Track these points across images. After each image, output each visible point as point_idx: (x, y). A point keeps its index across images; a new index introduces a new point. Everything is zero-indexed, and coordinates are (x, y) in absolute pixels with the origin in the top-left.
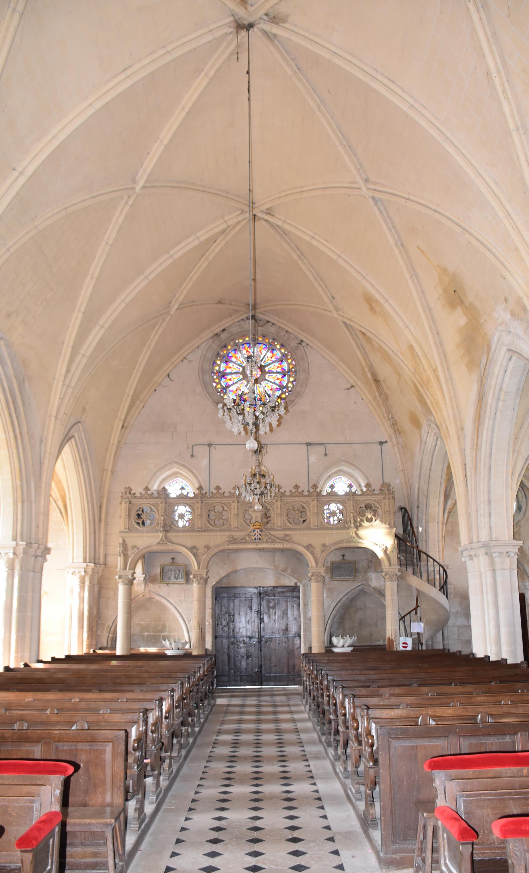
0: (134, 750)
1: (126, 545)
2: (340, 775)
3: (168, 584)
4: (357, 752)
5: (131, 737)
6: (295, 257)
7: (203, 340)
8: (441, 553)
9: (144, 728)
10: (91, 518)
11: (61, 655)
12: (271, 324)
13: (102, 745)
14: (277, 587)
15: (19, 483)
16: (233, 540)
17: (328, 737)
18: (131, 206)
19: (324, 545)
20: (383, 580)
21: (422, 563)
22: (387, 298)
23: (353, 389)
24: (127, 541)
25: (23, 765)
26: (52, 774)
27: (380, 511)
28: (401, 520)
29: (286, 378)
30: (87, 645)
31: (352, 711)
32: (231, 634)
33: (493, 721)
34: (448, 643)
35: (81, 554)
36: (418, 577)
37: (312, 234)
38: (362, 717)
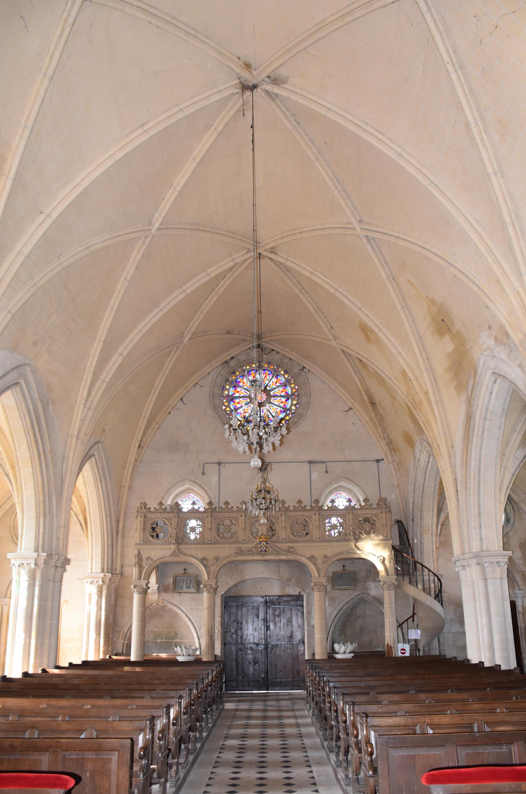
0: (141, 758)
1: (141, 557)
2: (342, 782)
3: (180, 593)
4: (357, 760)
5: (137, 745)
6: (297, 292)
7: (213, 367)
8: (435, 563)
9: (150, 736)
10: (109, 531)
11: (78, 661)
12: (276, 352)
13: (108, 754)
14: (282, 596)
15: (41, 498)
16: (240, 552)
17: (331, 742)
18: (148, 246)
19: (325, 556)
20: (381, 589)
21: (418, 573)
22: (381, 328)
23: (352, 411)
24: (142, 553)
25: (24, 778)
26: (53, 788)
27: (378, 525)
28: (398, 532)
29: (290, 401)
30: (103, 651)
31: (352, 718)
32: (239, 641)
33: (489, 730)
34: (444, 649)
35: (99, 565)
36: (414, 586)
37: (312, 270)
38: (362, 725)
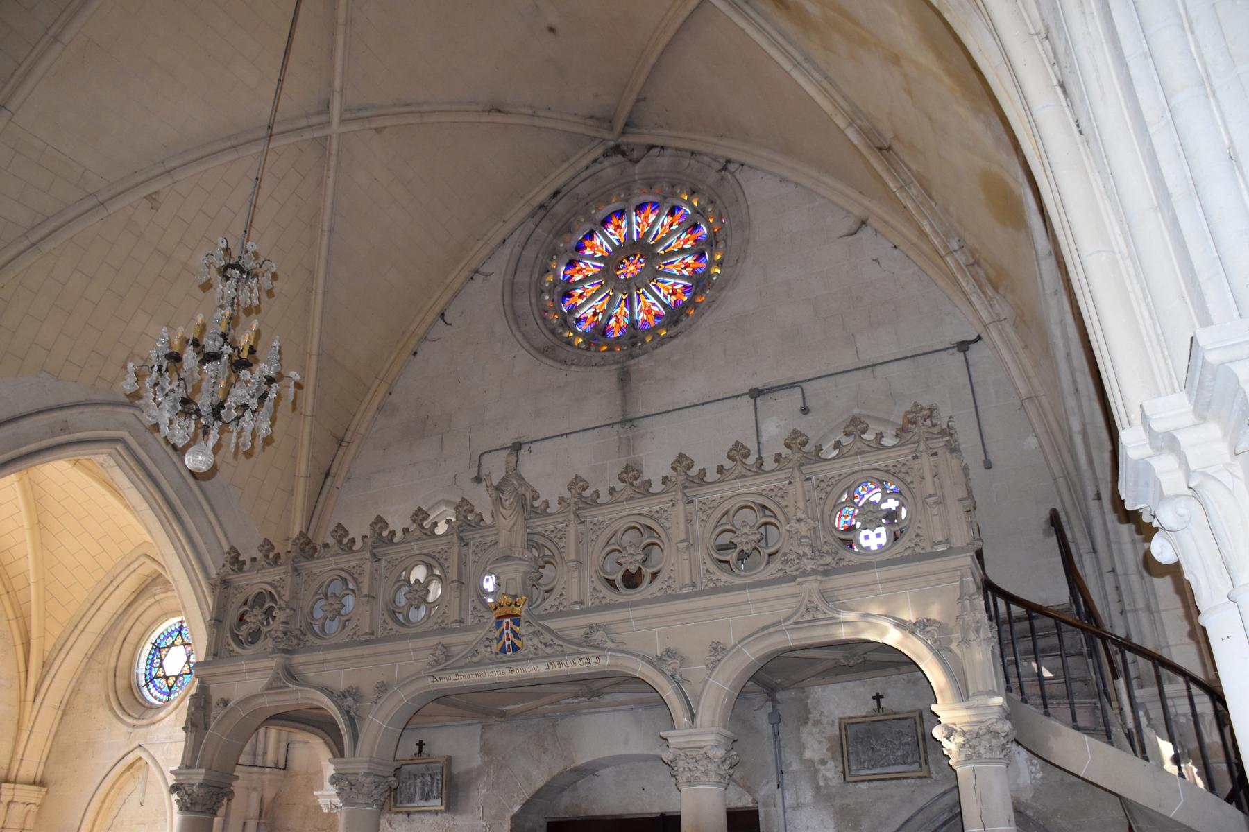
3: (409, 814)
7: (510, 226)
19: (717, 649)
